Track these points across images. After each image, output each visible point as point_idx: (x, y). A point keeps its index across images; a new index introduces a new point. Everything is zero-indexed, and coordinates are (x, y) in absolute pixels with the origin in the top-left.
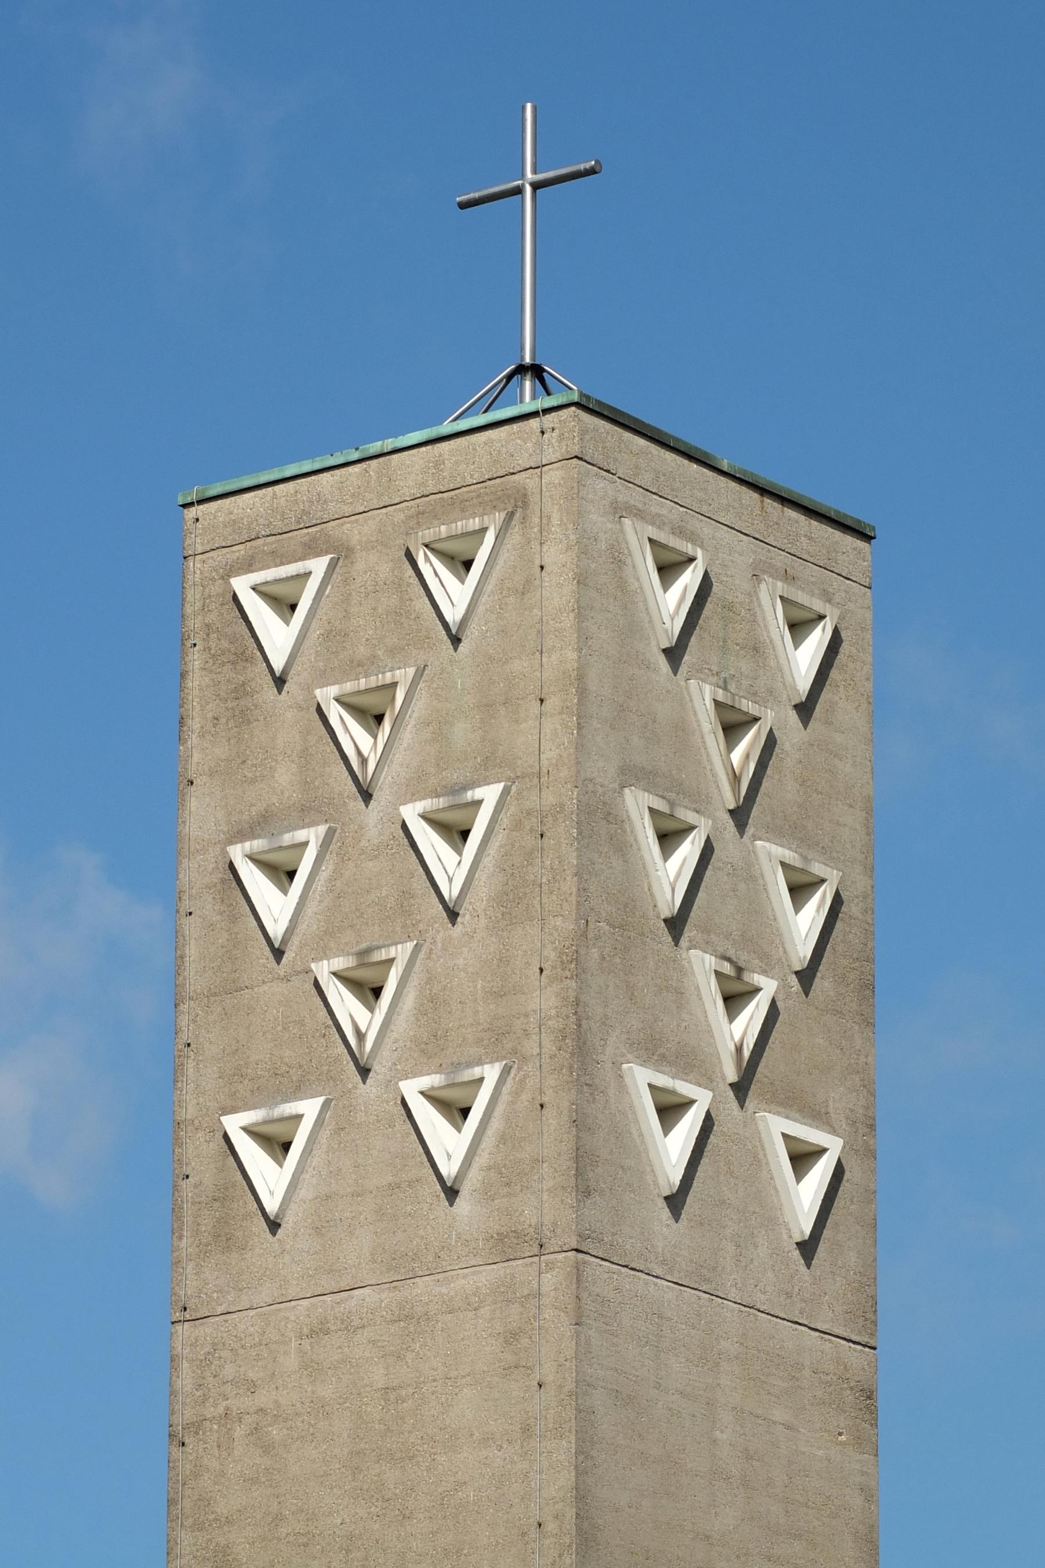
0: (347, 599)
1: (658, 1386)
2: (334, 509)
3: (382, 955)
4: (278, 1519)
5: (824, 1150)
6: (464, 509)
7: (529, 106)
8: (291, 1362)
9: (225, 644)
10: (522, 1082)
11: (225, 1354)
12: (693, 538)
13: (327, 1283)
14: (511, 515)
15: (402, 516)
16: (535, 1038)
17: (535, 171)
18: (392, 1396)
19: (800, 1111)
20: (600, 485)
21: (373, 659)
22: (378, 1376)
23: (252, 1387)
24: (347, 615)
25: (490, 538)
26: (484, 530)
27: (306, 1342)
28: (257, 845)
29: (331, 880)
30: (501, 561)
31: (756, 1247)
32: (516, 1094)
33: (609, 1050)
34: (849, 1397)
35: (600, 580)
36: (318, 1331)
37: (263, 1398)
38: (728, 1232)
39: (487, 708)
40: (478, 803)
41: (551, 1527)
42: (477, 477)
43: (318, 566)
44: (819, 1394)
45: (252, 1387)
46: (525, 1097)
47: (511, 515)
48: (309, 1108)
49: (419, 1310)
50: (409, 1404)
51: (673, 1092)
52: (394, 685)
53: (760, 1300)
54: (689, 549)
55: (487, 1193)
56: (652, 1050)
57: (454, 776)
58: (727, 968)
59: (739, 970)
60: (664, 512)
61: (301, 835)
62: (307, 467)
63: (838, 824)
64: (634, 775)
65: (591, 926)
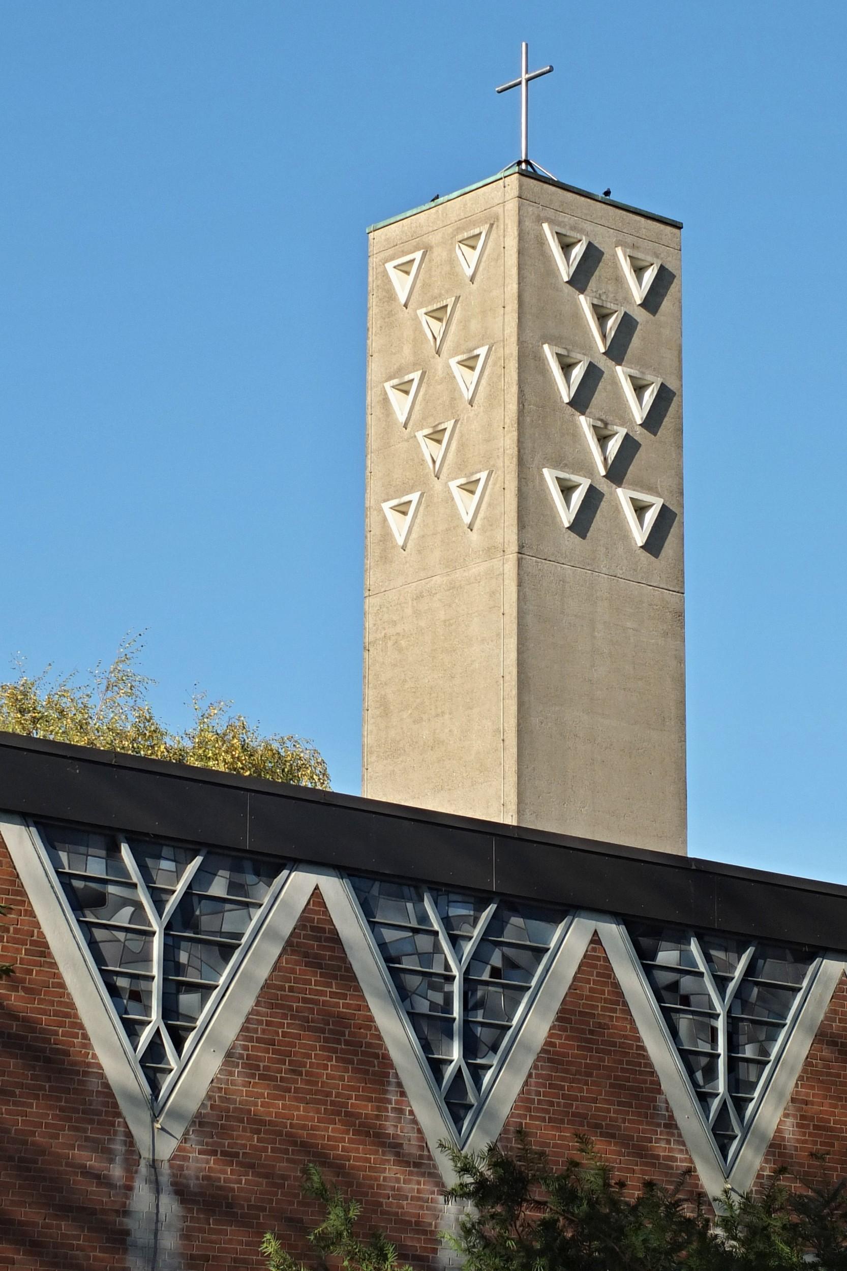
0: (430, 270)
1: (562, 613)
2: (425, 230)
3: (441, 427)
4: (405, 681)
5: (653, 504)
6: (474, 224)
7: (524, 44)
8: (409, 611)
9: (384, 294)
10: (496, 479)
11: (385, 609)
12: (581, 231)
13: (422, 574)
14: (492, 225)
15: (451, 230)
16: (501, 459)
17: (527, 72)
18: (447, 623)
19: (641, 487)
20: (530, 209)
21: (440, 295)
22: (442, 615)
23: (394, 623)
24: (431, 276)
25: (483, 237)
26: (480, 233)
27: (415, 602)
28: (395, 382)
29: (425, 394)
30: (488, 247)
31: (617, 549)
32: (495, 484)
33: (536, 462)
34: (669, 616)
35: (530, 252)
36: (419, 597)
37: (399, 629)
38: (602, 542)
39: (484, 313)
40: (478, 356)
41: (507, 678)
42: (480, 210)
43: (418, 255)
44: (652, 614)
45: (394, 623)
46: (498, 485)
47: (492, 225)
48: (414, 497)
49: (457, 584)
50: (454, 627)
51: (569, 480)
52: (447, 306)
53: (619, 573)
54: (579, 236)
55: (483, 530)
56: (558, 463)
57: (470, 345)
58: (599, 424)
59: (606, 424)
60: (566, 220)
61: (410, 377)
62: (415, 211)
63: (663, 357)
64: (546, 339)
65: (526, 407)
